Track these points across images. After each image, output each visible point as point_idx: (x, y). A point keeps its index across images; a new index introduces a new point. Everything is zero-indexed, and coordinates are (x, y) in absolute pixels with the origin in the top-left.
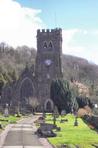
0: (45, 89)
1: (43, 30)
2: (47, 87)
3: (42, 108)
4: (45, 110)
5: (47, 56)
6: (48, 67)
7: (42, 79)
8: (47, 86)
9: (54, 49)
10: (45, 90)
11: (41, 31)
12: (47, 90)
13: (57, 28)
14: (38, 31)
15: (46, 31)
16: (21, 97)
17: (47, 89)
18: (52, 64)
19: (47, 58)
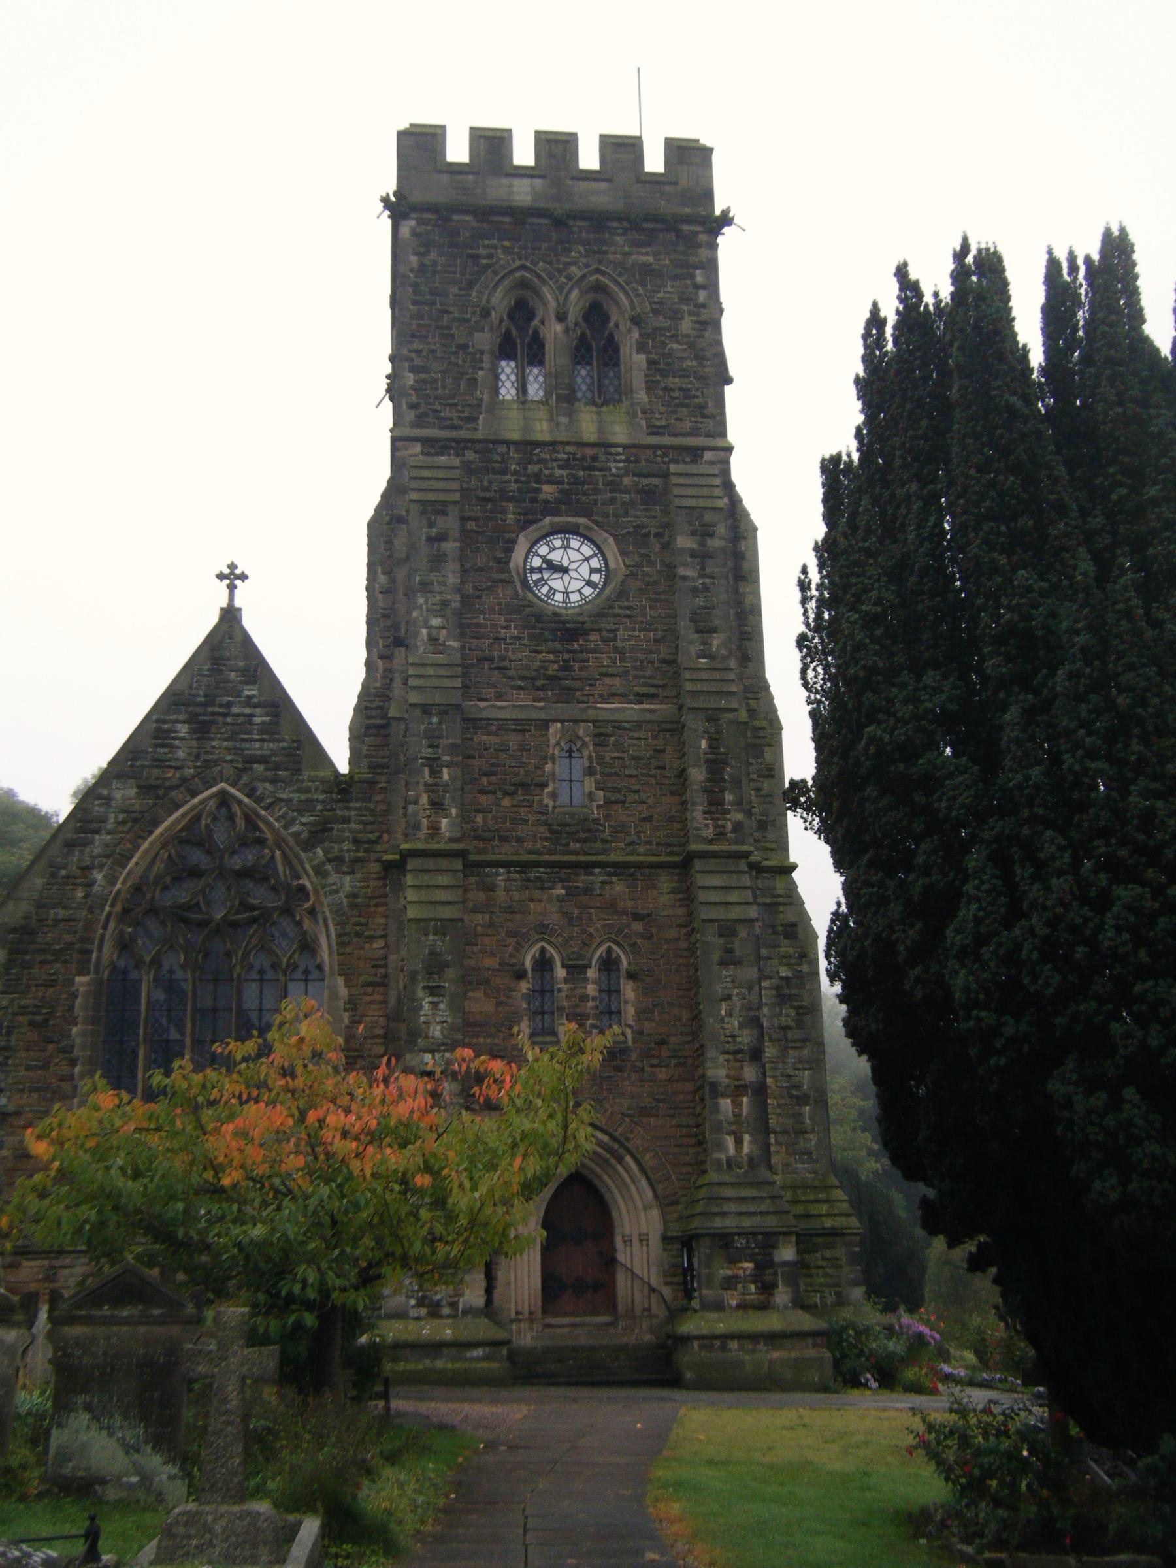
0: (520, 975)
1: (491, 144)
2: (544, 930)
3: (473, 1296)
4: (526, 1338)
5: (537, 477)
6: (567, 630)
7: (465, 817)
8: (554, 918)
9: (650, 387)
10: (524, 986)
11: (458, 151)
12: (544, 991)
13: (980, 276)
14: (419, 146)
15: (524, 154)
16: (414, 208)
17: (543, 964)
18: (622, 594)
19: (549, 509)
